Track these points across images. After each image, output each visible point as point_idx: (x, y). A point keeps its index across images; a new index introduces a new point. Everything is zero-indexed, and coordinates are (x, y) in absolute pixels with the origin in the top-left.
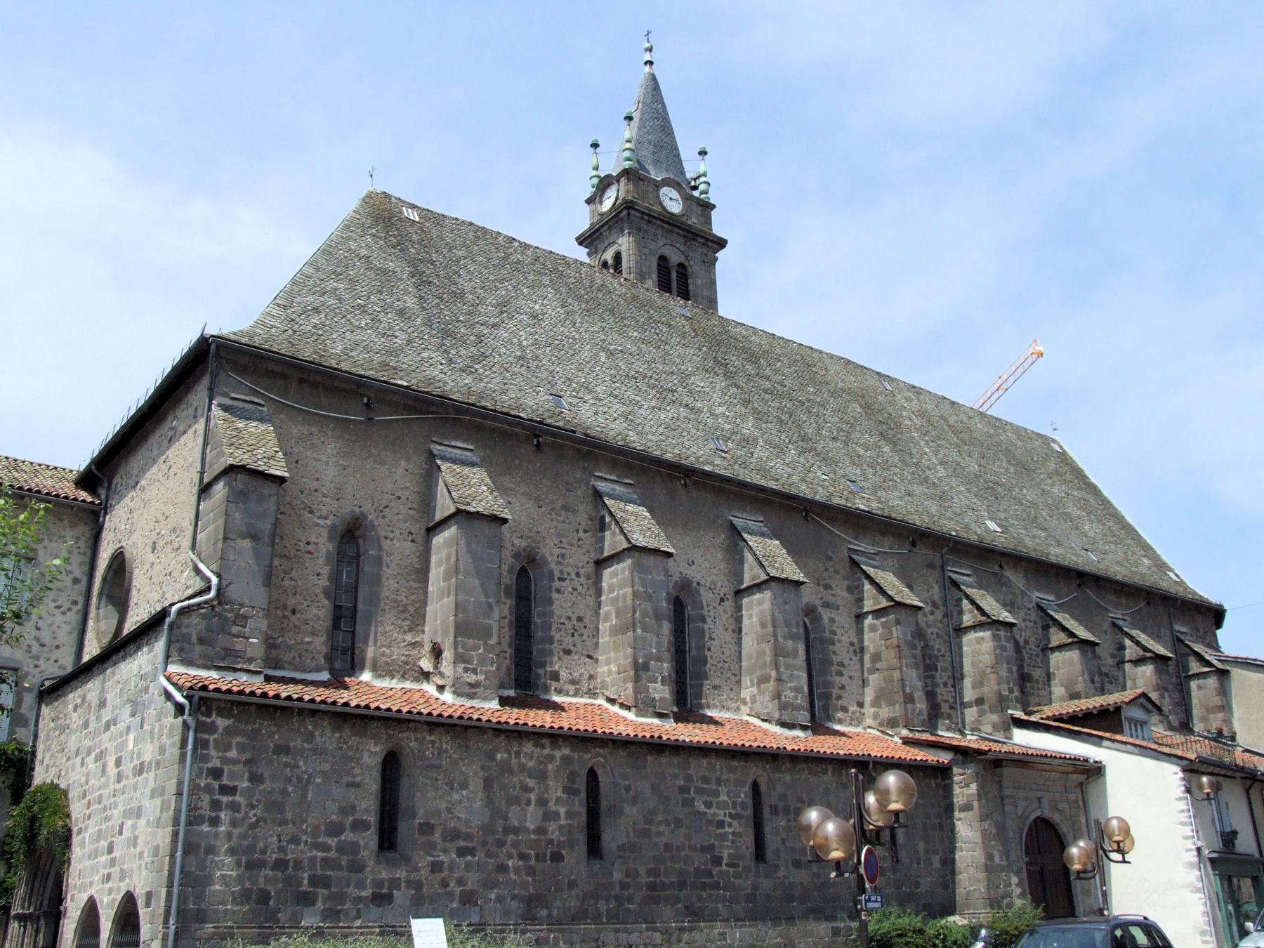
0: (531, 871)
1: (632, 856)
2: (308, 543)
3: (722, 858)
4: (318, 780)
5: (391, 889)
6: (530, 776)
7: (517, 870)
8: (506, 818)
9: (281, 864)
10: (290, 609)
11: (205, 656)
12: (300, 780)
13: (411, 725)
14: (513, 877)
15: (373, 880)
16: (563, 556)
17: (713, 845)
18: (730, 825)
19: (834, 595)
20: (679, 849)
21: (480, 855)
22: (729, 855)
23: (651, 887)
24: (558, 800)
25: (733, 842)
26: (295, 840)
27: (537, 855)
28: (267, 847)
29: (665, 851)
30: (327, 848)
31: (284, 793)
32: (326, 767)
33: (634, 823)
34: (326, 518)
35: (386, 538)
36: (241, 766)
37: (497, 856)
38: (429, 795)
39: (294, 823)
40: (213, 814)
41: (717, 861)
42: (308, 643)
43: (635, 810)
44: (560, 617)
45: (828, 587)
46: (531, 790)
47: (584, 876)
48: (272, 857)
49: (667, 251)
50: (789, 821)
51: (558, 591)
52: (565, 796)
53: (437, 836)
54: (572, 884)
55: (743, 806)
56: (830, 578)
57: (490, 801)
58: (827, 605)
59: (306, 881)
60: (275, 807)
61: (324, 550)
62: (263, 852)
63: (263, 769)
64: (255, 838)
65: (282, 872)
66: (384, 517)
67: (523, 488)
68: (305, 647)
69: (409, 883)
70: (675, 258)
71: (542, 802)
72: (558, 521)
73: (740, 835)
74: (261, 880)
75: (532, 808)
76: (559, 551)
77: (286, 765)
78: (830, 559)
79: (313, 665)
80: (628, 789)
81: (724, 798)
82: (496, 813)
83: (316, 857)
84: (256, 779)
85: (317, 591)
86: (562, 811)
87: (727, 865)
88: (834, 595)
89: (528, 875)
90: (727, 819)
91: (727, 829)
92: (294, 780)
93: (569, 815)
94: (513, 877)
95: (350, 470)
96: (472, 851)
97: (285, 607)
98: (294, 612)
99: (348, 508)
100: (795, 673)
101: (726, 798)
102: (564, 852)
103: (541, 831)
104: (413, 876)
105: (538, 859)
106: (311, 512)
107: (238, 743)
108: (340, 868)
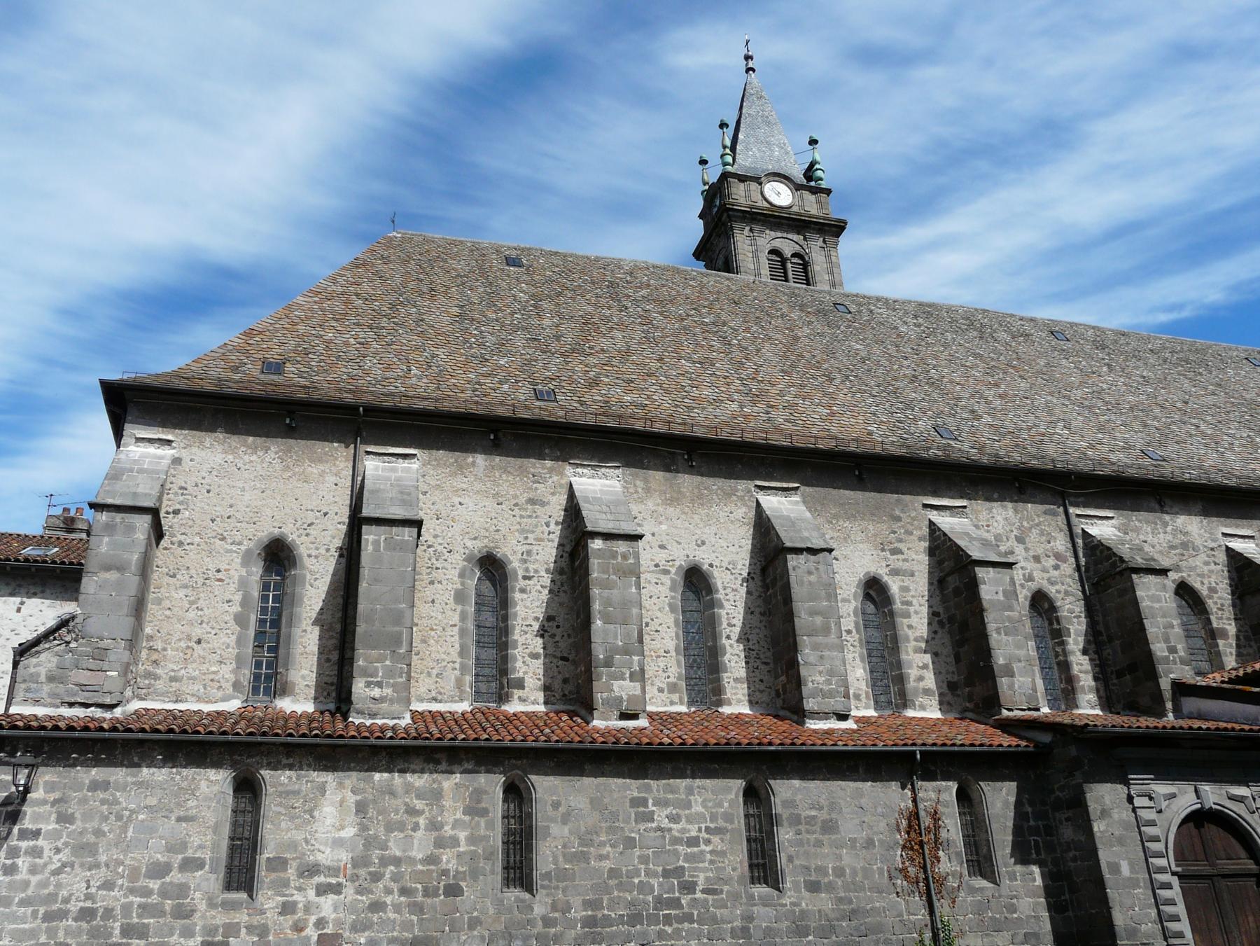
0: (417, 908)
1: (561, 885)
2: (218, 571)
3: (695, 883)
4: (141, 817)
5: (226, 935)
6: (418, 797)
7: (397, 908)
8: (384, 847)
9: (86, 914)
10: (195, 639)
11: (53, 695)
12: (119, 817)
13: (263, 749)
14: (392, 915)
15: (204, 927)
16: (529, 553)
17: (683, 868)
18: (708, 842)
19: (905, 560)
20: (630, 875)
21: (349, 892)
22: (707, 879)
23: (590, 922)
24: (457, 824)
25: (712, 862)
26: (108, 885)
27: (425, 890)
28: (71, 895)
29: (610, 877)
30: (147, 893)
31: (98, 833)
32: (153, 801)
33: (564, 846)
34: (240, 544)
35: (310, 556)
36: (48, 807)
37: (371, 892)
38: (283, 825)
39: (107, 865)
40: (8, 862)
41: (689, 887)
42: (214, 673)
43: (566, 830)
44: (524, 619)
45: (896, 551)
46: (419, 813)
47: (491, 911)
48: (74, 907)
49: (778, 244)
50: (799, 833)
51: (523, 591)
52: (467, 818)
53: (291, 872)
54: (474, 923)
55: (728, 818)
56: (900, 541)
57: (364, 828)
58: (895, 572)
59: (117, 932)
60: (84, 849)
61: (236, 578)
62: (66, 901)
63: (73, 808)
64: (59, 886)
65: (88, 922)
66: (307, 535)
67: (478, 486)
68: (212, 676)
69: (250, 929)
70: (788, 249)
71: (434, 826)
72: (522, 517)
73: (722, 854)
74: (61, 933)
75: (420, 833)
76: (525, 548)
77: (103, 802)
78: (899, 519)
79: (220, 694)
80: (556, 805)
81: (697, 808)
82: (369, 843)
83: (132, 903)
84: (65, 819)
85: (227, 618)
86: (462, 835)
87: (703, 891)
88: (905, 560)
89: (411, 913)
90: (704, 835)
91: (703, 847)
92: (112, 817)
93: (472, 840)
94: (392, 915)
95: (268, 492)
96: (336, 889)
97: (189, 638)
98: (199, 642)
99: (266, 530)
100: (826, 653)
101: (700, 809)
102: (463, 884)
103: (431, 860)
104: (256, 920)
105: (426, 893)
106: (223, 539)
107: (46, 783)
108: (162, 913)
